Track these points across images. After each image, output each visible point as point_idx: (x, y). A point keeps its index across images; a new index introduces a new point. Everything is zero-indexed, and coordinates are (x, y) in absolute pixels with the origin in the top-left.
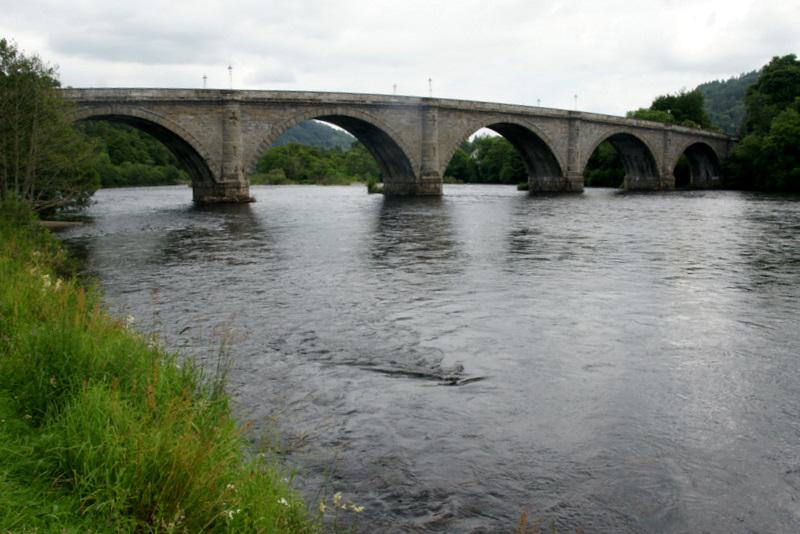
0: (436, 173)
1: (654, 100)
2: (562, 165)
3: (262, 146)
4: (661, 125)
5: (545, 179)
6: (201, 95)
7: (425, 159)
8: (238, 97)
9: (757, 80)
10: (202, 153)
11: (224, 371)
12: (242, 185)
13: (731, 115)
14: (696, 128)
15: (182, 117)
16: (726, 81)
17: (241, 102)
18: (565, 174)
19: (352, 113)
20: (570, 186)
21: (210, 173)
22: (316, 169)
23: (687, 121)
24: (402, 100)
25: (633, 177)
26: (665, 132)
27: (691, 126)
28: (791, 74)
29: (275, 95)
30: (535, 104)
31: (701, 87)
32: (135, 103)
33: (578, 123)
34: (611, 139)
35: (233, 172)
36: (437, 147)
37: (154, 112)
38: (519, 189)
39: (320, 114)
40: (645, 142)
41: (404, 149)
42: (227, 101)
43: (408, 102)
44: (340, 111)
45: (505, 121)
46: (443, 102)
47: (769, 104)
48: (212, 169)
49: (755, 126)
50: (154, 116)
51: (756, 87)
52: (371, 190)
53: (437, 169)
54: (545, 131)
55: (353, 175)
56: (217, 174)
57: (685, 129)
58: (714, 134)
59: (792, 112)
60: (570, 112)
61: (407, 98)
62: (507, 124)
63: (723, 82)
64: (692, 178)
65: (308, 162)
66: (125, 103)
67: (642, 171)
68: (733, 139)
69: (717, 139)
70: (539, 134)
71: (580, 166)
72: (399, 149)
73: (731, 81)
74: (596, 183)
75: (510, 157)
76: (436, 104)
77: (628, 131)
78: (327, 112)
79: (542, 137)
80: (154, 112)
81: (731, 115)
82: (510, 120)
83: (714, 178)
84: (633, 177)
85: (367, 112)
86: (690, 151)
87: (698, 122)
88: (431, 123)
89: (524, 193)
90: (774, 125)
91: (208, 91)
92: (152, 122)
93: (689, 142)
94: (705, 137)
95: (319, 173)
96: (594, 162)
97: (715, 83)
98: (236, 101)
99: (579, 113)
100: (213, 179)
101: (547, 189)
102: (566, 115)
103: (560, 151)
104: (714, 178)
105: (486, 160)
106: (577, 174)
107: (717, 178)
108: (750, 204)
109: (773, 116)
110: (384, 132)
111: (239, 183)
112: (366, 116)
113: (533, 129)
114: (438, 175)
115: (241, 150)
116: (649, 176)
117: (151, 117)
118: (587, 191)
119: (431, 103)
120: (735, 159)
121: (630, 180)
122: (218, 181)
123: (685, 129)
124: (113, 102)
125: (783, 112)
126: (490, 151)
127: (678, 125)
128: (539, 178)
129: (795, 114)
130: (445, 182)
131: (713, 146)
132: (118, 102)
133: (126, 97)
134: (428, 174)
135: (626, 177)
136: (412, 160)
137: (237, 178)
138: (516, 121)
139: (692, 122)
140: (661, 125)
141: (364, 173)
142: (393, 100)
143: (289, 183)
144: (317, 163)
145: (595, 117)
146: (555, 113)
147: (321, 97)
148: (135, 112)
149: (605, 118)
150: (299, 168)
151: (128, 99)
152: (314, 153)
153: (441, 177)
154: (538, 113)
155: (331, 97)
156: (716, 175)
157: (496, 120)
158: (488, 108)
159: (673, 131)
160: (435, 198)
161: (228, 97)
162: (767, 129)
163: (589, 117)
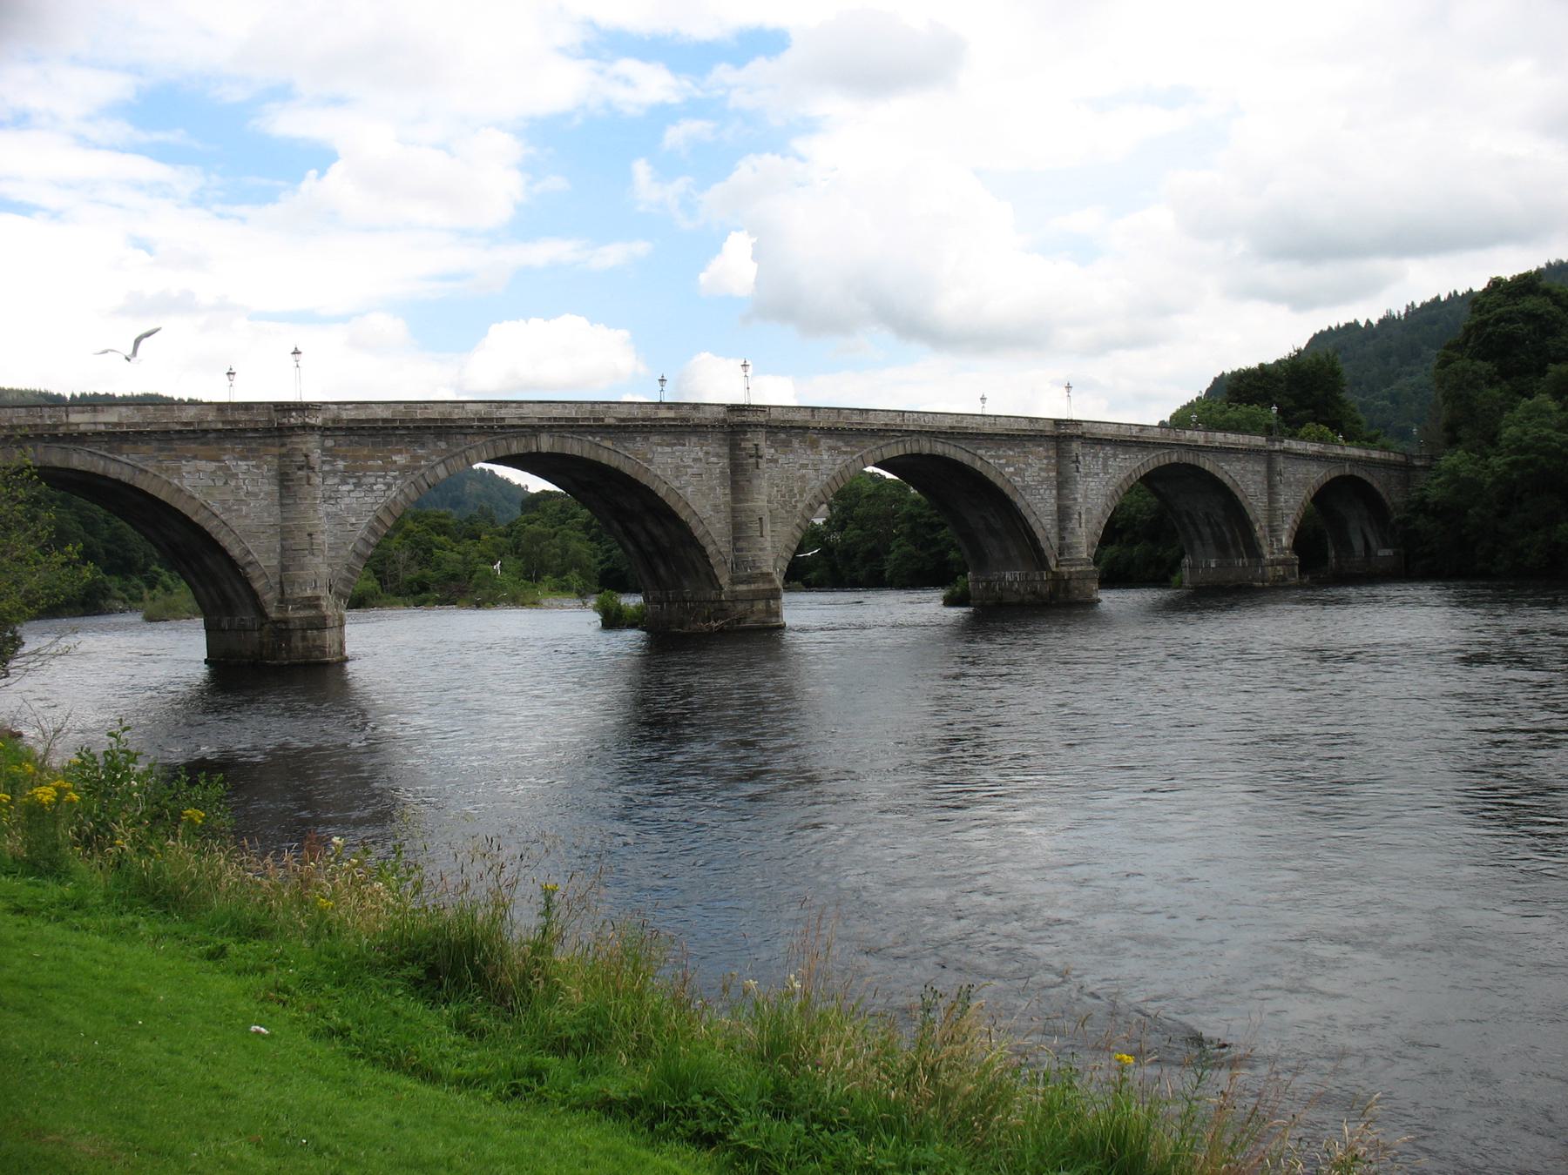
0: (767, 577)
1: (1217, 374)
2: (1044, 545)
3: (378, 519)
4: (1259, 441)
5: (1008, 576)
6: (229, 416)
7: (742, 544)
8: (317, 420)
9: (1461, 331)
10: (235, 552)
11: (47, 751)
12: (330, 623)
13: (1394, 398)
14: (1334, 442)
15: (187, 466)
16: (1375, 322)
17: (324, 430)
18: (1052, 563)
19: (574, 447)
20: (1067, 590)
21: (254, 595)
22: (449, 569)
23: (1310, 427)
24: (684, 412)
25: (1202, 563)
26: (1268, 457)
27: (1321, 439)
28: (1531, 317)
29: (584, 413)
30: (976, 409)
31: (1318, 339)
32: (79, 438)
33: (1076, 447)
34: (1150, 480)
35: (309, 593)
36: (766, 519)
37: (123, 458)
38: (950, 602)
39: (501, 454)
40: (1226, 479)
41: (693, 523)
42: (292, 428)
43: (697, 416)
44: (545, 444)
45: (916, 450)
46: (775, 414)
47: (1491, 383)
48: (258, 585)
49: (1463, 432)
50: (121, 466)
51: (1458, 347)
52: (612, 620)
53: (767, 568)
54: (998, 465)
55: (538, 579)
56: (269, 598)
57: (1312, 448)
58: (1375, 454)
59: (1545, 400)
60: (733, 408)
61: (696, 406)
62: (918, 456)
63: (73, 396)
64: (1332, 553)
65: (428, 551)
66: (55, 438)
67: (1222, 548)
68: (1417, 463)
69: (1385, 464)
70: (992, 476)
71: (1084, 537)
72: (683, 526)
73: (1387, 322)
74: (1115, 578)
75: (906, 527)
76: (762, 418)
77: (1189, 458)
78: (516, 447)
79: (999, 482)
80: (123, 458)
81: (1394, 398)
82: (926, 447)
83: (1381, 553)
84: (1202, 563)
85: (608, 444)
86: (1325, 497)
87: (1336, 426)
88: (752, 460)
89: (955, 613)
90: (1510, 432)
91: (247, 406)
92: (118, 482)
93: (1318, 475)
94: (1356, 461)
95: (454, 577)
96: (1115, 530)
97: (1352, 327)
98: (313, 427)
99: (1078, 423)
100: (260, 610)
101: (1015, 599)
102: (1049, 429)
103: (1039, 506)
104: (1381, 553)
105: (853, 532)
106: (1081, 562)
107: (1387, 552)
108: (1467, 617)
109: (1502, 409)
110: (646, 488)
111: (324, 618)
112: (608, 453)
113: (978, 465)
114: (772, 581)
115: (323, 539)
116: (1240, 556)
117: (114, 471)
118: (1110, 600)
119: (751, 418)
120: (1422, 507)
121: (1193, 568)
122: (274, 615)
123: (1312, 448)
124: (26, 437)
125: (1526, 402)
126: (858, 511)
127: (1292, 436)
128: (995, 575)
129: (1552, 405)
130: (788, 589)
131: (1376, 480)
132: (40, 437)
133: (56, 426)
134: (749, 580)
135: (1186, 561)
136: (710, 549)
137: (317, 607)
138: (940, 448)
139: (1323, 428)
140: (1259, 441)
141: (564, 573)
142: (664, 413)
143: (391, 605)
144: (451, 557)
145: (1112, 431)
146: (1025, 425)
147: (503, 413)
148: (79, 460)
149: (1135, 431)
150: (407, 568)
151: (62, 430)
152: (442, 529)
153: (779, 583)
154: (987, 430)
155: (525, 411)
156: (1385, 546)
157: (894, 450)
158: (877, 422)
159: (1286, 453)
160: (770, 633)
161: (295, 419)
162: (1492, 439)
163: (1100, 432)
